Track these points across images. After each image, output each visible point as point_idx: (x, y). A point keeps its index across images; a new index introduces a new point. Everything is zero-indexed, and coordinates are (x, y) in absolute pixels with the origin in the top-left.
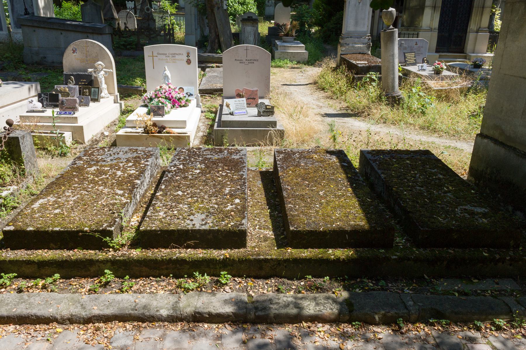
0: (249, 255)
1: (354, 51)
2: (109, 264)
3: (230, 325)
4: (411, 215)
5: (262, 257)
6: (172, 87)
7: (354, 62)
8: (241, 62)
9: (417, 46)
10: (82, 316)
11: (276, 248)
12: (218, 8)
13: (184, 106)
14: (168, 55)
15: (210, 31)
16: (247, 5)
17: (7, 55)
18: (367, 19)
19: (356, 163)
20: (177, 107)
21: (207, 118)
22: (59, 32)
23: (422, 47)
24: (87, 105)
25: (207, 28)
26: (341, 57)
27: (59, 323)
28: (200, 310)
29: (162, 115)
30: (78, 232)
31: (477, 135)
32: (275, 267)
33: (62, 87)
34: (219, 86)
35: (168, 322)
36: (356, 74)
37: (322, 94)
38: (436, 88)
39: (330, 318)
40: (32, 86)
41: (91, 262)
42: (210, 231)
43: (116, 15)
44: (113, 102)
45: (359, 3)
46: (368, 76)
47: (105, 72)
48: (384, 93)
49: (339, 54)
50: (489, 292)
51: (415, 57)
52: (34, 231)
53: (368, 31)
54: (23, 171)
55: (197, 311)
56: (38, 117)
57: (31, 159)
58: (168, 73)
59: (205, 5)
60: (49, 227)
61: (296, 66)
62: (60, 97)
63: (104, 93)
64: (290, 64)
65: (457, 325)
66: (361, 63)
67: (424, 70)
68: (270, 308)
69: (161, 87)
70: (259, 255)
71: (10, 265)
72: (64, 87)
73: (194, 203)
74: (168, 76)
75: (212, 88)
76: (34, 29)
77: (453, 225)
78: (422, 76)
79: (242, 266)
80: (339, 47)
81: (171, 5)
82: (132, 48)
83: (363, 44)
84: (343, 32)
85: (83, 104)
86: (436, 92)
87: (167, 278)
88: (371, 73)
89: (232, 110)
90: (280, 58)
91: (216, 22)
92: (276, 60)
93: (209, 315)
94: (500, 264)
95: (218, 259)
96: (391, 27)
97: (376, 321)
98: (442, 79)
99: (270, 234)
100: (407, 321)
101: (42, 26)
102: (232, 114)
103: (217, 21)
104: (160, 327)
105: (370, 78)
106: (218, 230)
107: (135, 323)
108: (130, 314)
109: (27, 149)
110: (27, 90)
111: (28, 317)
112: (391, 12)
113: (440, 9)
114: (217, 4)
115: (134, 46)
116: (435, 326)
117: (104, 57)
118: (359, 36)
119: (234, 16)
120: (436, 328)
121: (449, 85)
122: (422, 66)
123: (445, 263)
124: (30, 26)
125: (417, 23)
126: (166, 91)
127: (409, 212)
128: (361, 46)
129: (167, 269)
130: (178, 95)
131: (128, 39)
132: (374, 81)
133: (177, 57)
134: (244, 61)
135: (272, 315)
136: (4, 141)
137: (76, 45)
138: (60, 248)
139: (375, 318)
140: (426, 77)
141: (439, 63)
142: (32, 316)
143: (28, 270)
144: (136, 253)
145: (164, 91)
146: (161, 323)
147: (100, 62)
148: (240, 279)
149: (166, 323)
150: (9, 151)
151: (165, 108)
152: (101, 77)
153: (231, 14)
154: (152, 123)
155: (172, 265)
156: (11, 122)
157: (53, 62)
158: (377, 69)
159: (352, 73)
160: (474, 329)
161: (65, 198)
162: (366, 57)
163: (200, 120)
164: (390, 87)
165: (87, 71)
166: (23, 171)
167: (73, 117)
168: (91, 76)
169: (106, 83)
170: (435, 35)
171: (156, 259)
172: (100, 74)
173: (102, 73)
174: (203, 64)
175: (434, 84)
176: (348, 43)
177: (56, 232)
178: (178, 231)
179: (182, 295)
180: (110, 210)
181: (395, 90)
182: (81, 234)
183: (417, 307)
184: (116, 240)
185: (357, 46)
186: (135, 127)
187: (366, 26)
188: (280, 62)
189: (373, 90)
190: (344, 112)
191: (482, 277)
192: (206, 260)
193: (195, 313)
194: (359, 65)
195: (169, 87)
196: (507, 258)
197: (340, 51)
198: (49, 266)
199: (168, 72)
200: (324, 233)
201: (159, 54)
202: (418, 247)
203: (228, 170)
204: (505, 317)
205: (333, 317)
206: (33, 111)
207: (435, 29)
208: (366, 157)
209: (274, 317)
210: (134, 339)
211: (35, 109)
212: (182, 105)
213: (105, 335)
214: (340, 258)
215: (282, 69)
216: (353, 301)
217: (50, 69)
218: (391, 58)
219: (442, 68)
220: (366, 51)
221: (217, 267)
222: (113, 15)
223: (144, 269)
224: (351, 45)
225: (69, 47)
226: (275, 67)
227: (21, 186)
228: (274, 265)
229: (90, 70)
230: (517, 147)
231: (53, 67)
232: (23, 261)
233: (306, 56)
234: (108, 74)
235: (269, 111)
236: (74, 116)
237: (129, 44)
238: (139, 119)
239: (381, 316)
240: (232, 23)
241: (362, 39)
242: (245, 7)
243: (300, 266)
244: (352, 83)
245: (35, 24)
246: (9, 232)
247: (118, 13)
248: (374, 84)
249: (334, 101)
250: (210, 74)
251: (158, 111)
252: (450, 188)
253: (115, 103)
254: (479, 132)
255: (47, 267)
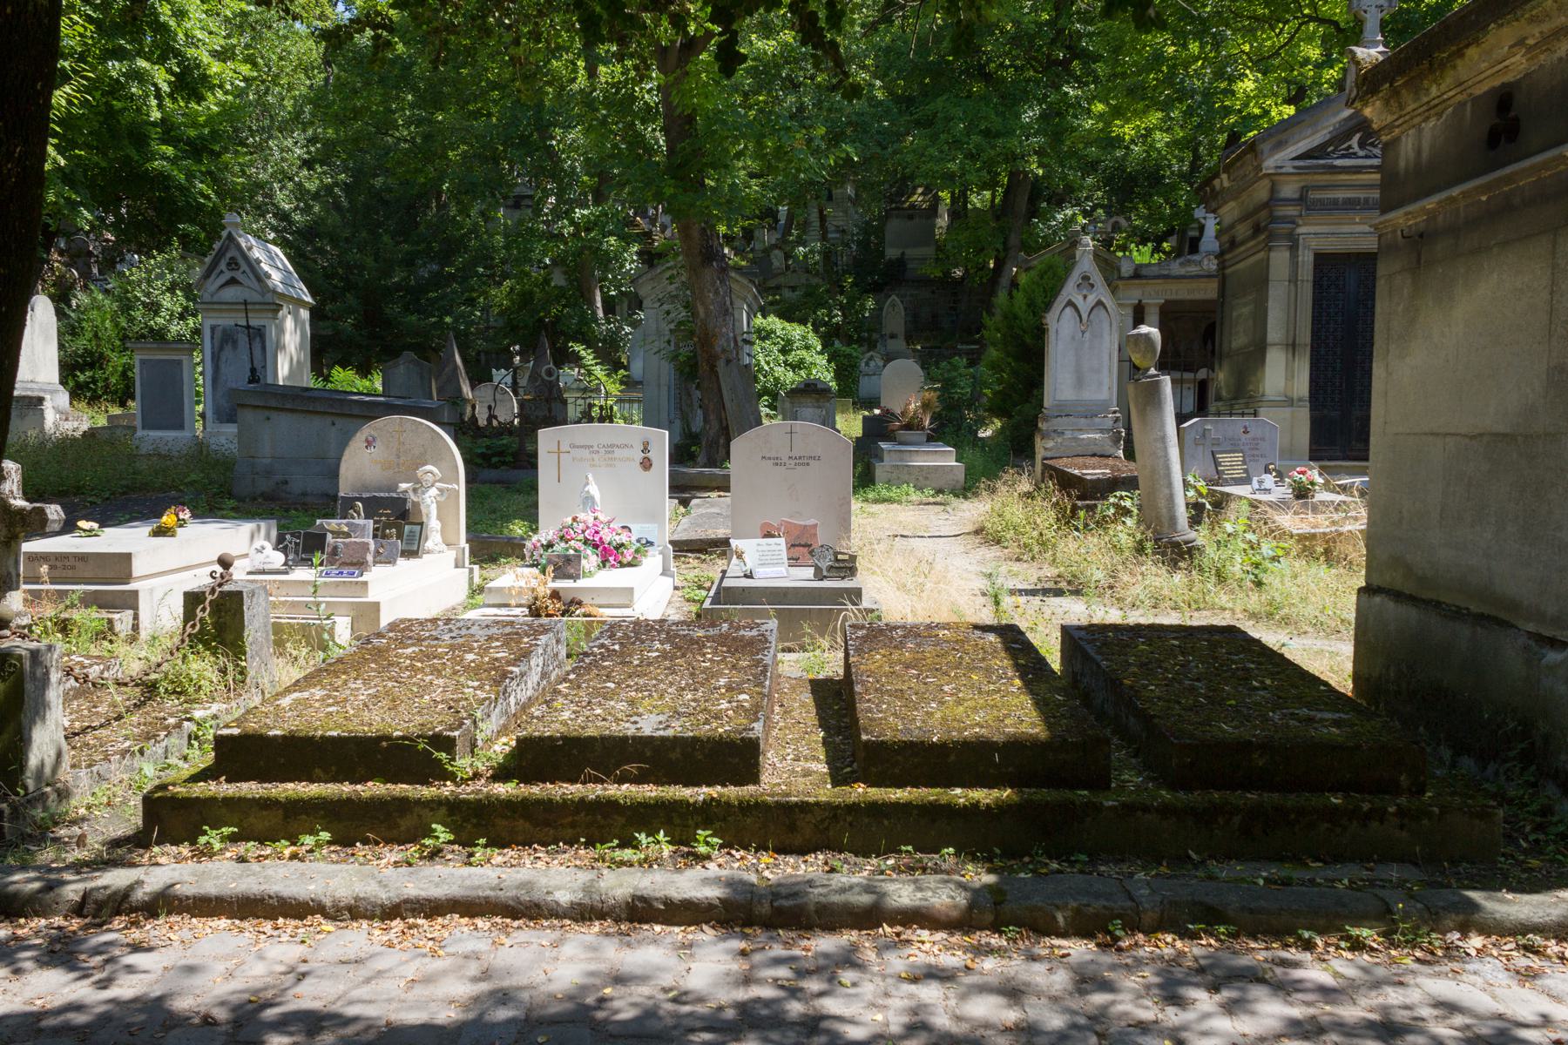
0: (762, 795)
1: (1079, 450)
2: (443, 810)
3: (713, 927)
4: (1156, 721)
5: (794, 799)
6: (602, 518)
7: (1076, 472)
8: (777, 462)
9: (1248, 436)
10: (379, 902)
11: (829, 786)
12: (728, 362)
13: (630, 565)
14: (596, 448)
15: (705, 418)
16: (808, 369)
17: (193, 477)
18: (1105, 371)
19: (1055, 662)
20: (613, 566)
21: (688, 601)
22: (329, 420)
23: (1263, 439)
24: (390, 561)
25: (699, 412)
26: (1044, 464)
27: (326, 916)
28: (645, 893)
29: (575, 577)
30: (380, 739)
31: (1360, 590)
32: (826, 823)
33: (333, 524)
34: (721, 533)
35: (571, 918)
36: (1079, 498)
37: (995, 551)
38: (1300, 531)
39: (947, 916)
40: (259, 528)
41: (403, 805)
42: (676, 741)
43: (466, 389)
44: (453, 565)
45: (1083, 332)
46: (1112, 500)
47: (441, 490)
48: (1150, 534)
49: (1039, 457)
50: (1346, 881)
51: (1244, 462)
52: (284, 737)
53: (1111, 399)
54: (241, 673)
55: (639, 893)
56: (275, 581)
57: (261, 649)
58: (593, 489)
59: (695, 356)
60: (316, 730)
61: (931, 500)
62: (330, 538)
63: (434, 540)
64: (915, 496)
65: (1256, 939)
66: (1095, 472)
67: (1268, 491)
68: (807, 893)
69: (574, 519)
70: (788, 795)
71: (224, 810)
72: (339, 525)
73: (643, 699)
74: (592, 498)
75: (704, 537)
76: (267, 413)
77: (1254, 736)
78: (1260, 502)
79: (749, 821)
80: (1038, 440)
81: (608, 375)
82: (504, 463)
83: (1102, 431)
84: (1046, 404)
85: (383, 559)
86: (1299, 541)
87: (572, 846)
88: (1118, 494)
89: (749, 567)
90: (888, 482)
91: (720, 390)
92: (879, 486)
93: (665, 904)
94: (1375, 825)
95: (691, 801)
96: (1153, 371)
97: (1059, 927)
98: (1315, 509)
99: (823, 768)
100: (1133, 927)
101: (288, 406)
102: (749, 576)
103: (725, 393)
104: (552, 927)
105: (1117, 506)
106: (694, 738)
107: (498, 920)
108: (486, 898)
109: (256, 624)
110: (248, 535)
111: (262, 900)
112: (1147, 336)
113: (1309, 348)
114: (724, 351)
115: (509, 459)
116: (1201, 939)
117: (439, 456)
118: (1090, 412)
119: (774, 396)
120: (1204, 942)
121: (1334, 523)
122: (1261, 482)
123: (1237, 820)
124: (258, 407)
125: (1251, 387)
126: (588, 527)
127: (1154, 717)
128: (1097, 436)
129: (573, 825)
130: (617, 538)
131: (494, 441)
132: (1127, 512)
133: (618, 453)
134: (785, 459)
135: (812, 908)
136: (210, 598)
137: (376, 429)
138: (334, 780)
139: (1054, 918)
140: (1270, 505)
141: (1303, 469)
142: (270, 897)
143: (258, 822)
144: (503, 790)
145: (582, 526)
146: (556, 922)
147: (429, 467)
148: (742, 853)
149: (568, 922)
150: (215, 625)
151: (584, 562)
152: (428, 501)
153: (765, 391)
154: (548, 592)
155: (587, 815)
156: (228, 559)
157: (304, 494)
158: (1131, 483)
159: (1069, 496)
160: (1297, 948)
161: (348, 692)
162: (1110, 461)
163: (669, 603)
164: (1165, 521)
165: (397, 487)
166: (241, 673)
167: (357, 583)
168: (405, 500)
169: (439, 518)
170: (1304, 415)
171: (550, 800)
172: (427, 495)
173: (433, 492)
174: (682, 490)
175: (1288, 521)
176: (1060, 429)
177: (332, 738)
178: (603, 739)
179: (605, 872)
180: (450, 708)
181: (1179, 527)
182: (384, 744)
183: (1158, 898)
184: (459, 762)
185: (1085, 436)
186: (506, 605)
187: (1106, 388)
188: (889, 490)
189: (1125, 532)
190: (1050, 585)
191: (1336, 857)
192: (663, 803)
193: (634, 897)
194: (1089, 477)
195: (595, 519)
196: (1390, 810)
197: (1042, 450)
198: (308, 815)
199: (595, 487)
200: (942, 748)
201: (573, 446)
202: (1173, 787)
203: (728, 652)
204: (1374, 923)
205: (955, 914)
206: (263, 572)
207: (1300, 400)
208: (1072, 638)
209: (816, 912)
210: (494, 942)
211: (267, 567)
212: (625, 561)
213: (430, 936)
214: (978, 802)
215: (895, 506)
216: (1005, 887)
217: (296, 509)
218: (1159, 445)
219: (1312, 484)
220: (1111, 451)
221: (690, 822)
222: (460, 390)
223: (522, 824)
224: (1068, 435)
225: (358, 434)
226: (876, 501)
227: (234, 704)
228: (822, 821)
229: (403, 486)
230: (1442, 600)
231: (304, 504)
232: (254, 798)
233: (960, 476)
234: (446, 494)
235: (846, 567)
236: (360, 579)
237: (501, 454)
238: (517, 584)
239: (1069, 913)
240: (767, 415)
241: (1097, 420)
242: (803, 373)
243: (886, 822)
244: (1067, 518)
245: (273, 403)
246: (231, 738)
247: (473, 388)
248: (1129, 522)
249: (1025, 565)
250: (702, 511)
251: (566, 566)
252: (1268, 682)
253: (457, 566)
254: (1364, 584)
255: (304, 817)
